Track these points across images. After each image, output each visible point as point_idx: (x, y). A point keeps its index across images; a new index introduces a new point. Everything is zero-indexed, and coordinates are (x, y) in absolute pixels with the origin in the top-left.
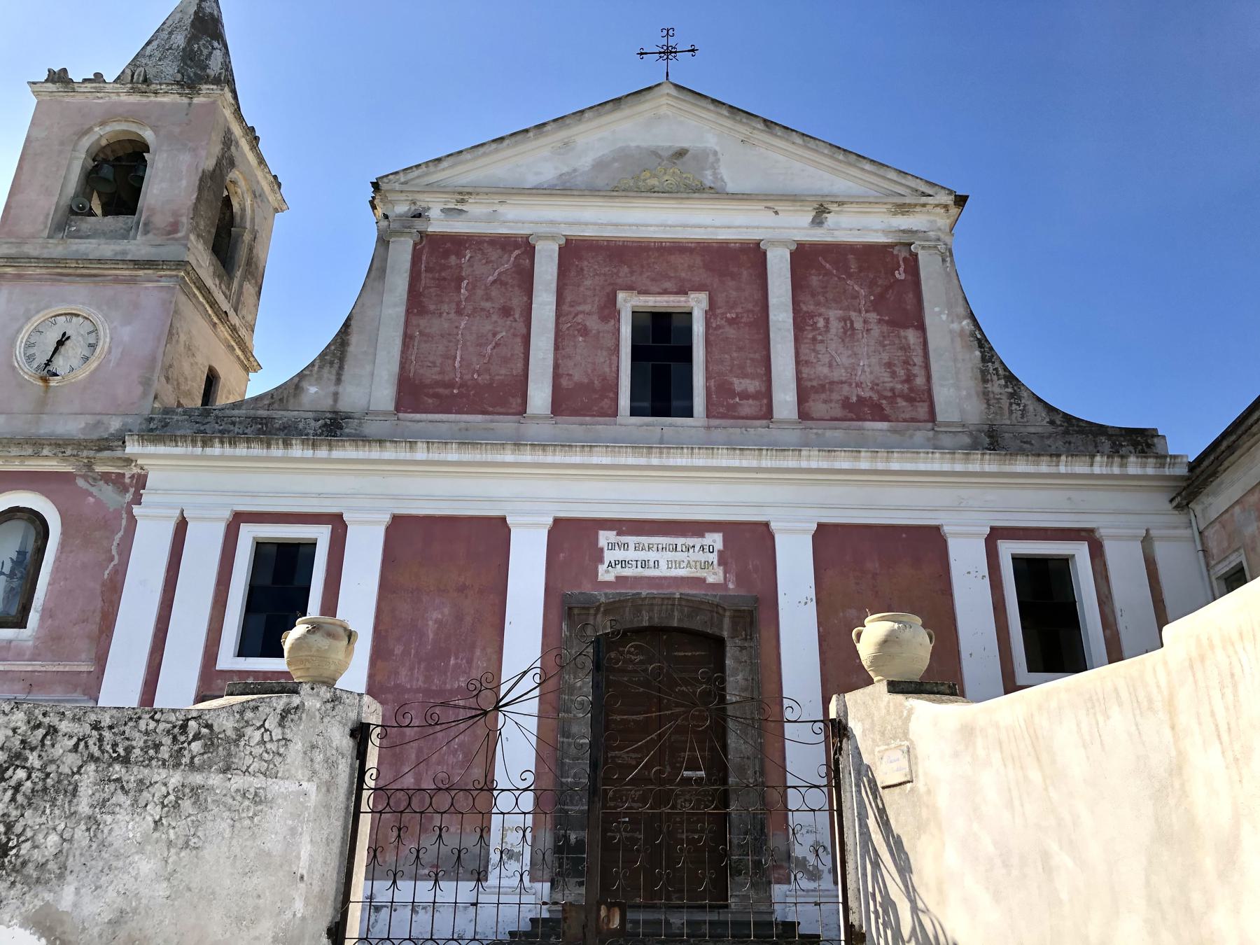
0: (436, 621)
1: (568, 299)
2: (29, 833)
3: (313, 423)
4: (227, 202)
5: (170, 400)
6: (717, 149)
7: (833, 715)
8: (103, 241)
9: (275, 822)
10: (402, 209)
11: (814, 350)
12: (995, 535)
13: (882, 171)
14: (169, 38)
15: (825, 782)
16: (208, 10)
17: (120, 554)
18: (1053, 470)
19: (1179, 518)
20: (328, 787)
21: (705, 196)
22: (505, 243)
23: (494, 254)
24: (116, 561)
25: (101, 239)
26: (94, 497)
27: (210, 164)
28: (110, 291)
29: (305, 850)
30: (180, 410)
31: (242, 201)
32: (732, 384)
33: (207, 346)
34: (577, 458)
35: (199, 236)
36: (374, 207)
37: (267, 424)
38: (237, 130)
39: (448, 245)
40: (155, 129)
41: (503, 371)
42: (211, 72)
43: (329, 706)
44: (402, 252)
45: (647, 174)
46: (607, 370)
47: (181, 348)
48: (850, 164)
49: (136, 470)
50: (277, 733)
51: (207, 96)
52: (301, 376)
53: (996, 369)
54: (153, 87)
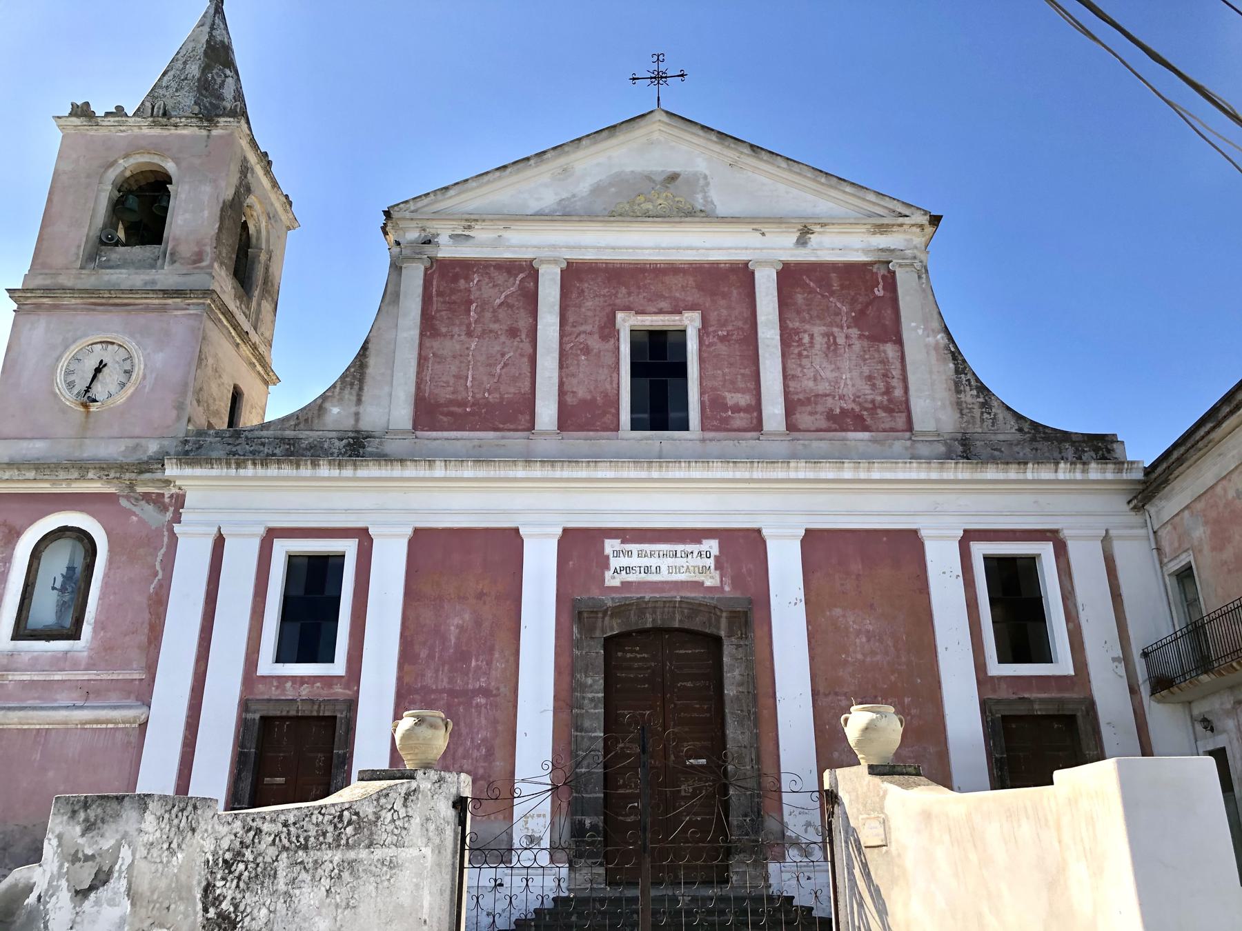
0: (457, 626)
1: (571, 320)
2: (249, 910)
3: (337, 443)
4: (245, 226)
5: (201, 421)
6: (707, 172)
7: (826, 787)
8: (132, 271)
9: (405, 878)
10: (413, 235)
11: (800, 365)
12: (969, 536)
13: (861, 193)
14: (184, 68)
15: (819, 839)
16: (219, 38)
17: (163, 570)
18: (1021, 476)
19: (1135, 518)
20: (439, 849)
21: (697, 219)
22: (510, 267)
23: (500, 278)
24: (160, 576)
25: (130, 270)
26: (136, 515)
27: (229, 194)
28: (142, 319)
29: (427, 901)
30: (212, 432)
31: (257, 222)
32: (725, 398)
33: (232, 364)
34: (583, 473)
35: (222, 264)
36: (386, 233)
37: (292, 444)
38: (252, 158)
39: (457, 269)
40: (177, 162)
41: (512, 390)
42: (228, 105)
43: (437, 785)
44: (414, 277)
45: (642, 198)
46: (608, 387)
47: (210, 371)
48: (831, 187)
49: (174, 490)
50: (402, 813)
51: (224, 128)
52: (324, 397)
53: (968, 380)
54: (173, 120)
